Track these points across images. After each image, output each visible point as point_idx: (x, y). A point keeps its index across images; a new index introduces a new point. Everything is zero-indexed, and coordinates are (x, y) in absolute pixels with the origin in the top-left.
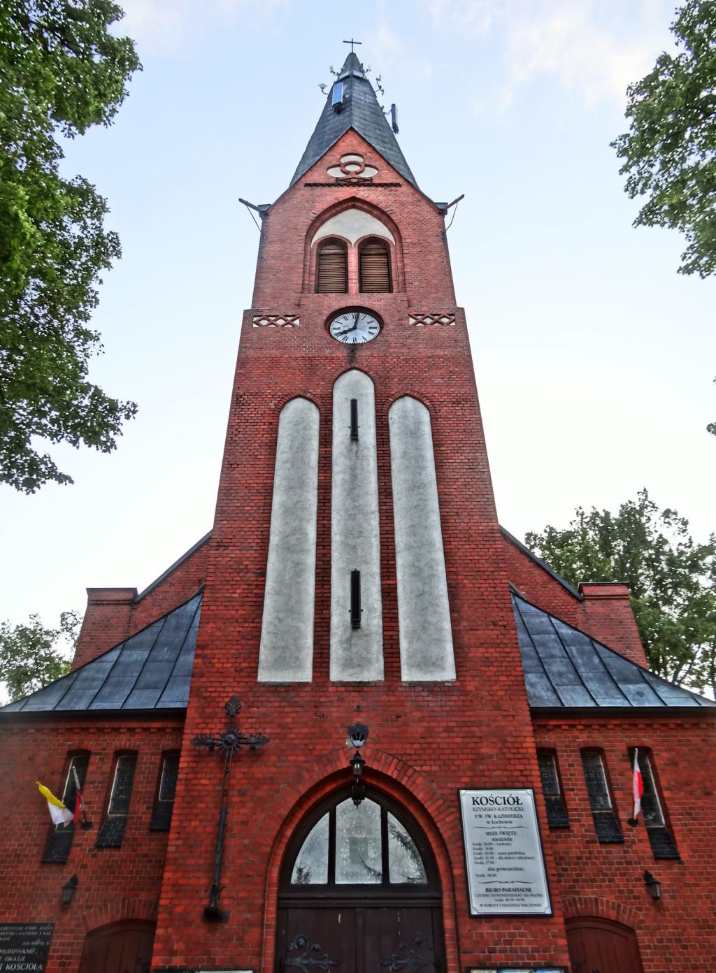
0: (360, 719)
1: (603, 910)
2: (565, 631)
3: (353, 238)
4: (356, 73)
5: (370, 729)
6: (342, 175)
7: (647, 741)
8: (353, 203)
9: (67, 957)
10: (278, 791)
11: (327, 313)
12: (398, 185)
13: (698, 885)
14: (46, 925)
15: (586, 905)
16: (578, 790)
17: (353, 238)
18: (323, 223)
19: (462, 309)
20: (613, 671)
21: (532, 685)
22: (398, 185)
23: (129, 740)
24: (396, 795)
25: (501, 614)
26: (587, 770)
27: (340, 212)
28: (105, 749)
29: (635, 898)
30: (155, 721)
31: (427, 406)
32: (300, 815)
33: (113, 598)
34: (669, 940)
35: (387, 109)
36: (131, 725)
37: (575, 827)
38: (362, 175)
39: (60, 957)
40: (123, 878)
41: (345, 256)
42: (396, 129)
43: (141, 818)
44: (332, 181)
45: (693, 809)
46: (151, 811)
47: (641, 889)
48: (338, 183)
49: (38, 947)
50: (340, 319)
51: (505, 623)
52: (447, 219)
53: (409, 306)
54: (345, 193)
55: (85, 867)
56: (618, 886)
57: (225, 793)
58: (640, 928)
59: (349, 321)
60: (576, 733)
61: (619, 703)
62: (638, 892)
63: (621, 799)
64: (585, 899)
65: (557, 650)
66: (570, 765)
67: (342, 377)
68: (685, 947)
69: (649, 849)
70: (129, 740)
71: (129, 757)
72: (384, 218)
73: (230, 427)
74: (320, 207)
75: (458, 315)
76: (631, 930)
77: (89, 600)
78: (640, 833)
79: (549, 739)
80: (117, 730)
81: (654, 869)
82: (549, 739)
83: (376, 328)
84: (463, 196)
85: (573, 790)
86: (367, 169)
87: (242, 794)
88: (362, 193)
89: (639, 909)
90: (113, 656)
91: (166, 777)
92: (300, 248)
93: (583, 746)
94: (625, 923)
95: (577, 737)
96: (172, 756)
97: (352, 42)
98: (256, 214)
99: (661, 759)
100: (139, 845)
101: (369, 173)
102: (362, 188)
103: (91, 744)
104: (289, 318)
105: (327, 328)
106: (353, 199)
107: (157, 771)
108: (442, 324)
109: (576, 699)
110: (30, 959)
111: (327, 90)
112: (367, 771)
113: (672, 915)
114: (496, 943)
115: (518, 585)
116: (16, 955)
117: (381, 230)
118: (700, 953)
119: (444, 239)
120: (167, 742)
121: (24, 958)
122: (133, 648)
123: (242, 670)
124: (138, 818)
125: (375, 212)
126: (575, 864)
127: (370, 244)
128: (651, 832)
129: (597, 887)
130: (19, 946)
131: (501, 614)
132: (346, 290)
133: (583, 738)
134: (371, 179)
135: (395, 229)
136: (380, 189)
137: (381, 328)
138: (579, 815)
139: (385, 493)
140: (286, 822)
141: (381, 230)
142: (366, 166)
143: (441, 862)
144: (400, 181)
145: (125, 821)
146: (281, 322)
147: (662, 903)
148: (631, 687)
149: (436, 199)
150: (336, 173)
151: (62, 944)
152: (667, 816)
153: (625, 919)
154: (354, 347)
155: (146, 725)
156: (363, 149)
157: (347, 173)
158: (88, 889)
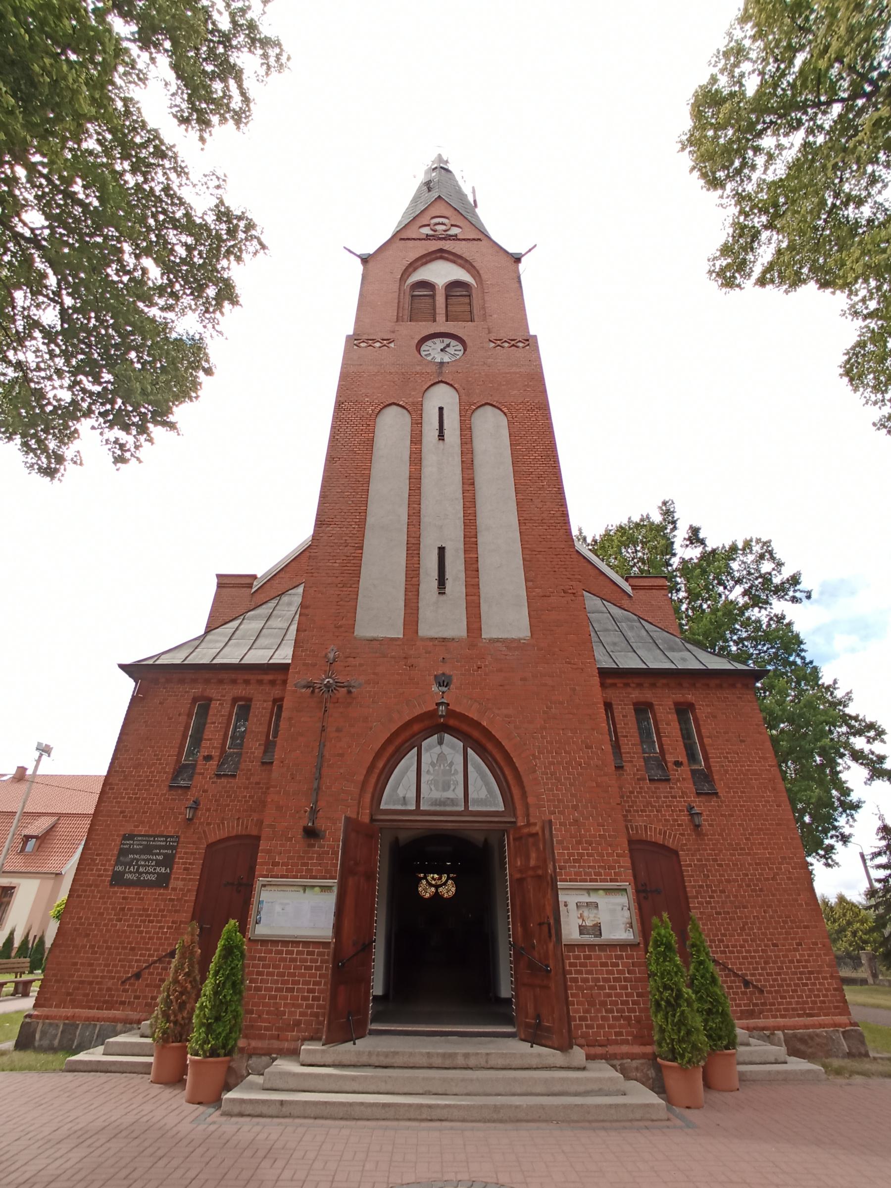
1: (651, 835)
5: (455, 680)
6: (431, 233)
7: (690, 697)
9: (190, 864)
10: (371, 728)
11: (419, 338)
12: (479, 239)
13: (732, 816)
14: (172, 837)
15: (637, 831)
16: (631, 736)
18: (415, 270)
19: (535, 336)
20: (659, 642)
23: (245, 689)
25: (571, 583)
26: (639, 722)
28: (224, 696)
29: (679, 825)
30: (267, 674)
31: (505, 414)
33: (237, 582)
34: (708, 860)
36: (246, 677)
38: (449, 233)
39: (185, 863)
40: (238, 801)
41: (433, 297)
42: (476, 205)
43: (254, 753)
44: (424, 237)
45: (729, 753)
46: (263, 747)
47: (685, 818)
48: (428, 237)
49: (165, 855)
50: (429, 343)
51: (574, 591)
52: (521, 267)
53: (489, 333)
54: (434, 245)
55: (205, 791)
56: (665, 815)
57: (323, 729)
59: (439, 344)
60: (629, 690)
61: (668, 665)
62: (681, 820)
63: (669, 745)
64: (636, 826)
65: (611, 625)
66: (625, 713)
68: (720, 865)
69: (692, 786)
70: (245, 689)
72: (467, 266)
73: (333, 427)
74: (413, 256)
75: (530, 342)
76: (676, 853)
77: (218, 584)
78: (685, 771)
81: (695, 802)
84: (535, 246)
85: (626, 736)
86: (453, 228)
87: (338, 730)
88: (447, 245)
89: (683, 835)
92: (395, 287)
93: (635, 701)
94: (670, 845)
95: (631, 694)
96: (278, 702)
98: (359, 260)
99: (702, 711)
100: (251, 774)
101: (454, 231)
102: (448, 242)
103: (212, 692)
105: (419, 351)
106: (441, 250)
107: (268, 715)
108: (517, 347)
109: (630, 662)
110: (159, 863)
112: (451, 714)
113: (709, 840)
114: (566, 861)
116: (148, 860)
117: (463, 275)
118: (733, 870)
119: (519, 282)
120: (276, 692)
121: (154, 863)
122: (252, 618)
123: (341, 627)
124: (252, 753)
125: (460, 261)
126: (628, 797)
128: (693, 772)
129: (646, 816)
131: (571, 583)
133: (636, 695)
134: (456, 235)
137: (465, 350)
138: (631, 757)
139: (469, 484)
141: (463, 275)
142: (452, 225)
143: (516, 791)
145: (239, 755)
147: (702, 830)
148: (675, 654)
149: (511, 250)
150: (426, 231)
151: (185, 853)
152: (706, 759)
153: (670, 843)
155: (260, 677)
156: (448, 212)
157: (435, 231)
158: (208, 810)
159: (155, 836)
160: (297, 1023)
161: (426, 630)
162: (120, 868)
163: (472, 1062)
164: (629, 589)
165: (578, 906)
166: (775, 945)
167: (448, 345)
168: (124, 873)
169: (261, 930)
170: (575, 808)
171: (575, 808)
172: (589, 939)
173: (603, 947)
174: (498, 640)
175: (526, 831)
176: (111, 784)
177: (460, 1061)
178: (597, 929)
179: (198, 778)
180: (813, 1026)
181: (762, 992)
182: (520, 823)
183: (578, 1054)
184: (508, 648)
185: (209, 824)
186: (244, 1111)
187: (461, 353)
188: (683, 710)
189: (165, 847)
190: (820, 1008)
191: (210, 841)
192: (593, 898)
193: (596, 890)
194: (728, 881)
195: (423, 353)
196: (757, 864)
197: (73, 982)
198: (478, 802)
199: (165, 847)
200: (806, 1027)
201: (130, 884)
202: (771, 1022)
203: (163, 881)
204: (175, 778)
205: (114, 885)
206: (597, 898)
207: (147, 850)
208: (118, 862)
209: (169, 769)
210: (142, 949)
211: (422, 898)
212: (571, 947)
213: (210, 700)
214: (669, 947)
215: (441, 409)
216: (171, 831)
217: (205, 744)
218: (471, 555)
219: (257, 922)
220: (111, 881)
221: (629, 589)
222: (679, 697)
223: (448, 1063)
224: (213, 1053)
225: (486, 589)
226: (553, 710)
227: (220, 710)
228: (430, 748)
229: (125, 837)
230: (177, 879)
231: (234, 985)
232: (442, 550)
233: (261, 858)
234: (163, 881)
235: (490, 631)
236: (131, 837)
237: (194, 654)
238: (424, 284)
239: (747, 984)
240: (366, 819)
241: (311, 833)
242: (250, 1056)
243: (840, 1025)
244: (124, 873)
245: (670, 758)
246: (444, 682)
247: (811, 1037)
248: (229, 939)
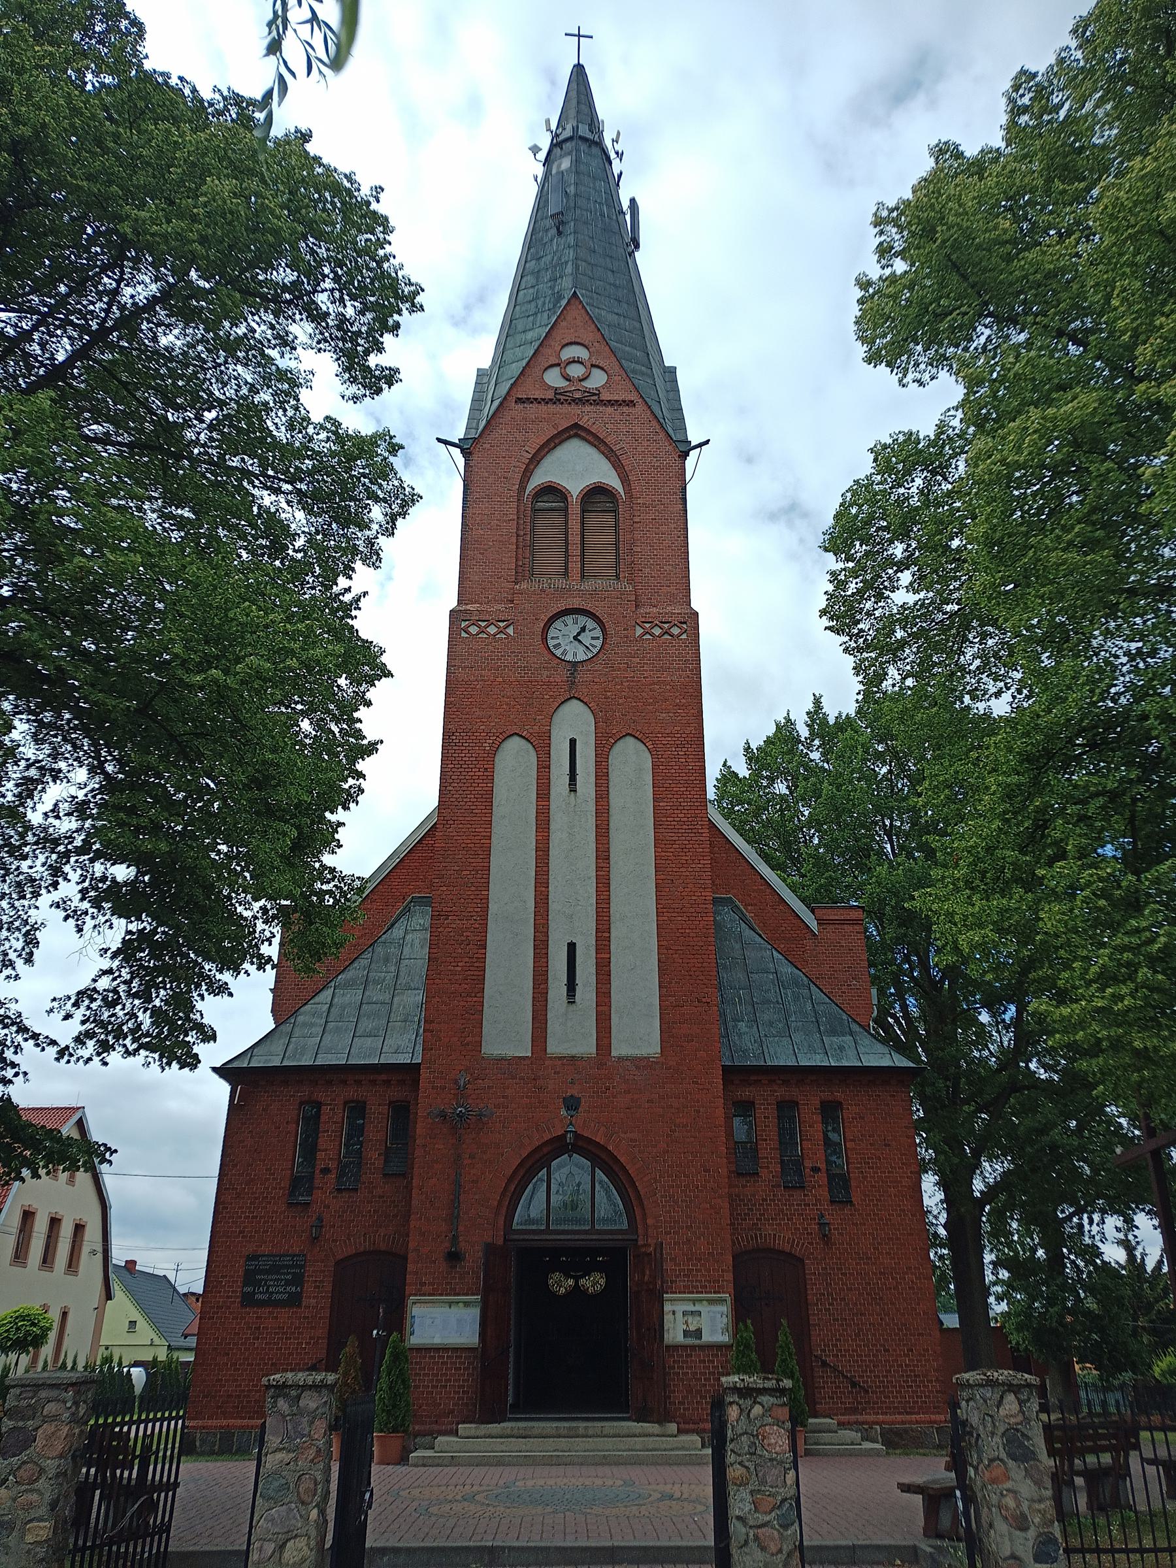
0: (574, 1091)
2: (787, 969)
3: (575, 487)
4: (584, 131)
6: (561, 383)
7: (838, 1095)
8: (576, 431)
12: (631, 404)
17: (575, 487)
21: (740, 1035)
22: (631, 404)
24: (604, 1156)
27: (560, 443)
32: (522, 1173)
35: (625, 205)
37: (763, 1173)
44: (550, 395)
50: (558, 624)
54: (567, 415)
58: (809, 1259)
66: (766, 1113)
67: (561, 708)
71: (358, 1109)
76: (801, 1261)
78: (822, 1178)
79: (745, 1093)
80: (344, 1082)
82: (745, 1093)
83: (598, 638)
84: (707, 442)
87: (472, 1157)
90: (326, 995)
91: (392, 1124)
97: (579, 36)
98: (456, 452)
102: (587, 408)
103: (320, 1096)
104: (502, 624)
110: (288, 1283)
111: (542, 156)
112: (577, 1135)
114: (677, 1276)
115: (746, 906)
127: (597, 494)
130: (278, 1273)
132: (566, 574)
133: (781, 1092)
135: (624, 480)
136: (610, 409)
139: (603, 856)
140: (510, 1180)
142: (592, 366)
144: (633, 396)
146: (492, 630)
153: (797, 1251)
154: (575, 664)
159: (281, 1256)
160: (452, 1411)
161: (555, 1047)
162: (249, 1289)
163: (590, 1432)
164: (813, 925)
165: (685, 1313)
166: (886, 1350)
167: (583, 629)
168: (254, 1293)
169: (415, 1340)
170: (689, 1228)
171: (689, 1228)
172: (690, 1341)
173: (702, 1347)
174: (627, 1058)
175: (643, 1250)
176: (223, 1203)
177: (581, 1431)
178: (698, 1333)
179: (318, 1193)
180: (911, 1422)
181: (867, 1392)
182: (640, 1243)
183: (673, 1427)
184: (638, 1068)
185: (335, 1241)
186: (424, 1463)
187: (598, 643)
188: (830, 1110)
189: (292, 1266)
190: (920, 1408)
191: (339, 1257)
192: (697, 1308)
193: (701, 1301)
194: (850, 1289)
195: (551, 643)
196: (881, 1273)
197: (221, 1396)
198: (605, 1221)
199: (292, 1266)
200: (903, 1423)
201: (262, 1304)
202: (872, 1418)
203: (294, 1300)
204: (292, 1194)
205: (246, 1306)
206: (703, 1308)
207: (275, 1269)
208: (245, 1284)
209: (286, 1184)
210: (282, 1364)
211: (554, 1295)
212: (676, 1347)
213: (319, 1105)
214: (747, 1346)
215: (573, 742)
216: (296, 1250)
217: (320, 1155)
218: (603, 956)
219: (412, 1334)
220: (242, 1302)
221: (813, 925)
222: (826, 1095)
223: (572, 1433)
224: (395, 1430)
225: (617, 997)
226: (676, 1134)
227: (333, 1117)
228: (560, 1167)
229: (249, 1258)
230: (310, 1297)
231: (403, 1381)
232: (572, 947)
233: (409, 1278)
234: (294, 1300)
235: (620, 1048)
236: (254, 1257)
237: (291, 1047)
238: (551, 491)
239: (854, 1384)
240: (500, 1242)
241: (454, 1257)
242: (416, 1437)
243: (935, 1422)
244: (254, 1293)
245: (808, 1164)
246: (572, 1104)
247: (906, 1431)
248: (395, 1348)
